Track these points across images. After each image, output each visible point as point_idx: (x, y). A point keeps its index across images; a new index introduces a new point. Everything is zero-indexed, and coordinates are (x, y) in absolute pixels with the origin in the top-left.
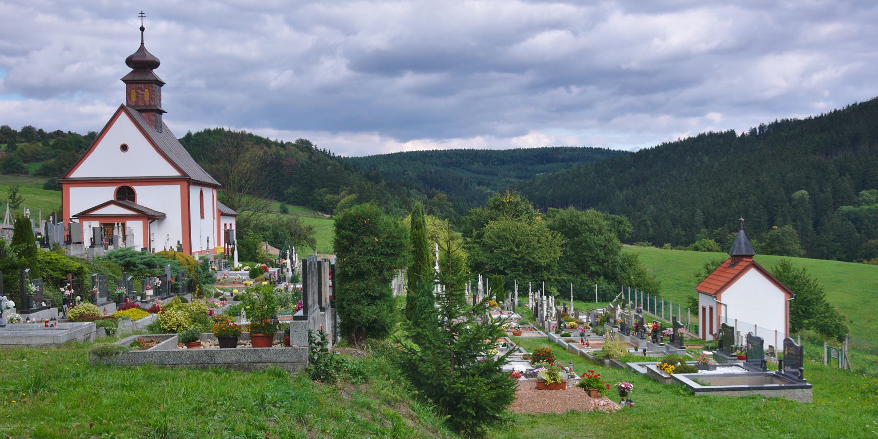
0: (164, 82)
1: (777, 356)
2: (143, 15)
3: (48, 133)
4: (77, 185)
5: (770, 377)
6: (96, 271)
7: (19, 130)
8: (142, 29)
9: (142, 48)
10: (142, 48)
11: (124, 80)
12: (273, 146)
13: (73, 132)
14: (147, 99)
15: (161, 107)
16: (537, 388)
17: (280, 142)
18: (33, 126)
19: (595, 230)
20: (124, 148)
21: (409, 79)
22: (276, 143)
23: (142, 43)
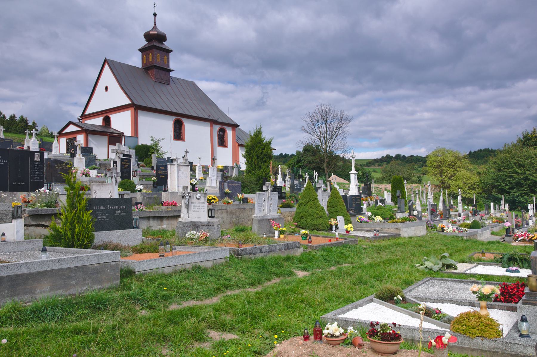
0: (172, 49)
2: (155, 5)
3: (407, 156)
4: (88, 119)
6: (405, 220)
7: (394, 156)
8: (155, 15)
9: (155, 27)
10: (155, 27)
11: (140, 50)
13: (418, 155)
14: (150, 60)
15: (169, 67)
16: (516, 311)
18: (400, 154)
20: (106, 88)
23: (155, 24)
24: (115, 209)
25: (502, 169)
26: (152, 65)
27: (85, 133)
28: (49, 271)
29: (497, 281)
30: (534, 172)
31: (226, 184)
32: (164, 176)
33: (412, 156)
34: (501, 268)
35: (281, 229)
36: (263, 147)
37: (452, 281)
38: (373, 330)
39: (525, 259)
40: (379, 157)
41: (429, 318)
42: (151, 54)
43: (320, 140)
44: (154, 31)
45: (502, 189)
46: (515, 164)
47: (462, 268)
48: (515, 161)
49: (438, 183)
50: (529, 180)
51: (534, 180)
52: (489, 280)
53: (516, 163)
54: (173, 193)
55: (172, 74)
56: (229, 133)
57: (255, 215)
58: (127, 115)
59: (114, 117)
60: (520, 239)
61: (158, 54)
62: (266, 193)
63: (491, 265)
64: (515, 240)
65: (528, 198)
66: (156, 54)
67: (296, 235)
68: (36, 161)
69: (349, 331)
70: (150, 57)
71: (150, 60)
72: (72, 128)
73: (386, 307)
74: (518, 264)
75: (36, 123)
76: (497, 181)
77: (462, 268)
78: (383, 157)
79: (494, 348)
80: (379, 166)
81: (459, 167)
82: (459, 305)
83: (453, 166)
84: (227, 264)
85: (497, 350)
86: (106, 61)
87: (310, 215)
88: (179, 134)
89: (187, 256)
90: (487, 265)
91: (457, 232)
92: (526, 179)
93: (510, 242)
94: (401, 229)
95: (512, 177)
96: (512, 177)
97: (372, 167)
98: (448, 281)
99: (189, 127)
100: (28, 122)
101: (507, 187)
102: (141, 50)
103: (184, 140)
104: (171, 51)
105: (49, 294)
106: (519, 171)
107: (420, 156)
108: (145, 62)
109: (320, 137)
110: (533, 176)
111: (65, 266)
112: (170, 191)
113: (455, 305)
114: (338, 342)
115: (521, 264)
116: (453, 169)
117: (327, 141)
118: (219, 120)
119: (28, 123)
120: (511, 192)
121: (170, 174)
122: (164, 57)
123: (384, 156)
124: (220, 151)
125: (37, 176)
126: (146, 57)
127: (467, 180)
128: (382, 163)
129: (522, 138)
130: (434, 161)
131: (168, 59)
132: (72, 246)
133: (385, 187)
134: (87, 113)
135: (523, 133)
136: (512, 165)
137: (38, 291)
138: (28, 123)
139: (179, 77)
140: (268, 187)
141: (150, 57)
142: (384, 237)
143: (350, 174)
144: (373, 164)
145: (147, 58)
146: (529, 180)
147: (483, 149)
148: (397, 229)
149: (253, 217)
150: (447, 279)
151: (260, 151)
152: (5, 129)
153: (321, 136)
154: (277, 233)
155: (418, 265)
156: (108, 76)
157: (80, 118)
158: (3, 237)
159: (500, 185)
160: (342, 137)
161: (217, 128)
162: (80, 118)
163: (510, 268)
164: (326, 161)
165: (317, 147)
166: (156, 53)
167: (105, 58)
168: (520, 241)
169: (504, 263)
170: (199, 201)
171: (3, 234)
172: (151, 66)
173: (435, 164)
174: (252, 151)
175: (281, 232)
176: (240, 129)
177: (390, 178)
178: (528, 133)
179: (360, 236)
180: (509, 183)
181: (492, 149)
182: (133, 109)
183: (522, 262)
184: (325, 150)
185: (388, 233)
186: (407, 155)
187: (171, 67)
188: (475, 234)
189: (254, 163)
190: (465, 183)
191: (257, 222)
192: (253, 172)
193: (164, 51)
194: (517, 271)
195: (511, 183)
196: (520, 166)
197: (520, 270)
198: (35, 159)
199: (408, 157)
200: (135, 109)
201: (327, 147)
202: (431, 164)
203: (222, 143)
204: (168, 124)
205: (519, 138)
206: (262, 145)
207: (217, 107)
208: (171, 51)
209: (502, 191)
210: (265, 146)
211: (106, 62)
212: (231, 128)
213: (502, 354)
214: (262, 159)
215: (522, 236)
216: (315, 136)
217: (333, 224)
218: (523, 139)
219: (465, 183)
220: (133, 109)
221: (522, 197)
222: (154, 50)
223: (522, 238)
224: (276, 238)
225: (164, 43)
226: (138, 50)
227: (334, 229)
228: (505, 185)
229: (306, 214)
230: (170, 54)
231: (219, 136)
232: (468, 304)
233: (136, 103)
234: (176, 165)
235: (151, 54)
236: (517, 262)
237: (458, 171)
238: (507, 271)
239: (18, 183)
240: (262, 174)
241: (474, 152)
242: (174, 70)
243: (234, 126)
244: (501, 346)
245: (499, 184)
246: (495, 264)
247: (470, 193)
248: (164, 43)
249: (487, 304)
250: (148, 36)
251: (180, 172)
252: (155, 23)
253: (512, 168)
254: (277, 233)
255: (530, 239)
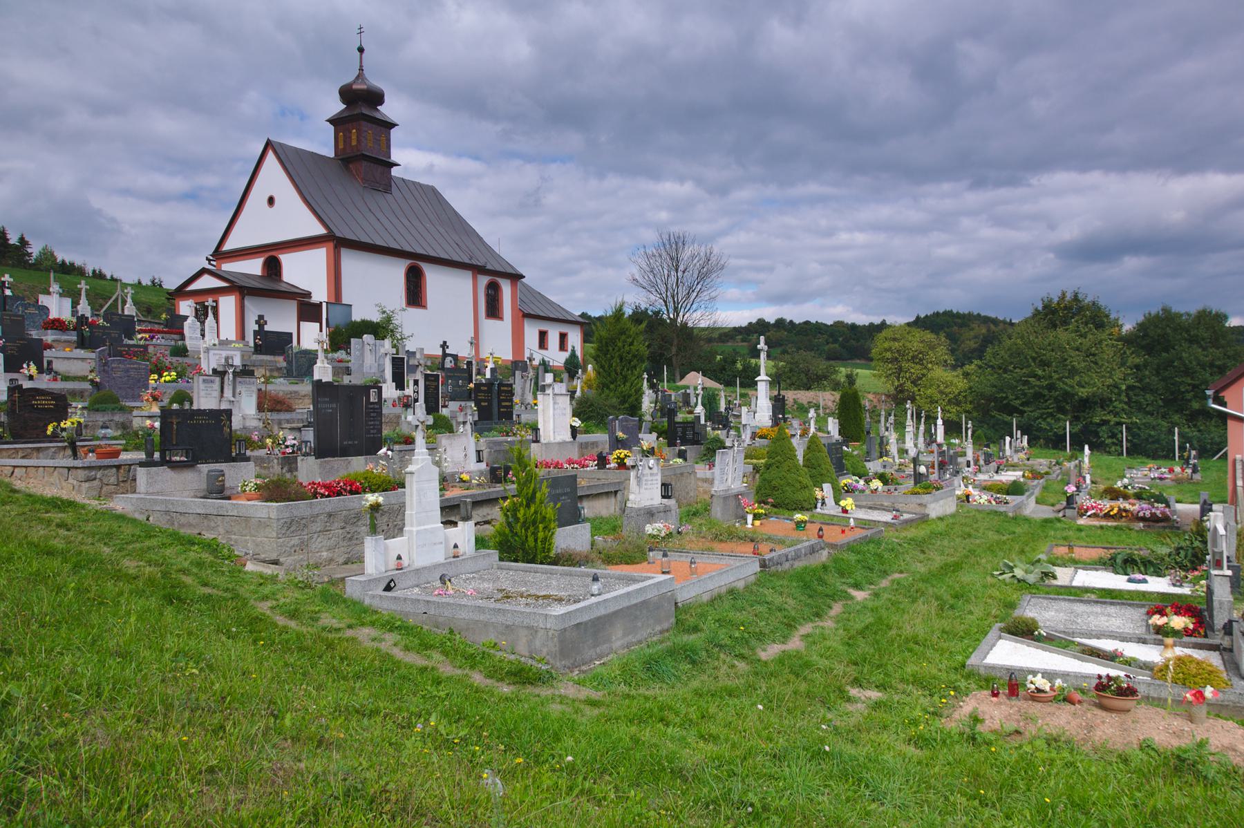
1: (1021, 408)
2: (362, 30)
5: (24, 470)
7: (772, 322)
8: (361, 50)
9: (361, 76)
10: (361, 76)
11: (331, 121)
12: (1001, 324)
13: (819, 321)
14: (354, 143)
15: (390, 157)
17: (1008, 321)
18: (784, 317)
19: (1203, 339)
20: (271, 201)
21: (1131, 263)
22: (1004, 322)
23: (361, 69)
24: (559, 494)
25: (1011, 368)
26: (359, 153)
27: (238, 294)
28: (621, 609)
29: (1129, 599)
30: (1067, 375)
31: (617, 422)
32: (486, 404)
33: (807, 323)
34: (1113, 574)
35: (756, 511)
36: (630, 340)
37: (1065, 600)
38: (1101, 683)
39: (1150, 562)
40: (744, 324)
41: (1113, 663)
42: (354, 131)
43: (665, 302)
44: (361, 84)
45: (1008, 405)
46: (1034, 359)
47: (1063, 576)
48: (1034, 355)
49: (892, 391)
50: (1056, 389)
51: (1065, 390)
52: (1116, 597)
53: (1036, 358)
54: (548, 445)
55: (395, 172)
56: (506, 288)
57: (715, 489)
58: (318, 257)
59: (287, 259)
60: (1089, 513)
61: (370, 131)
62: (730, 452)
63: (1097, 570)
64: (1082, 515)
65: (1053, 421)
66: (366, 131)
67: (772, 519)
68: (373, 403)
69: (1057, 684)
70: (354, 137)
71: (354, 143)
72: (207, 282)
73: (1028, 646)
74: (1139, 569)
75: (26, 239)
76: (1002, 390)
77: (1063, 576)
78: (750, 323)
79: (1222, 701)
80: (743, 341)
81: (931, 362)
82: (1123, 641)
83: (921, 360)
84: (758, 583)
85: (1227, 703)
86: (269, 145)
87: (788, 484)
88: (415, 295)
89: (721, 574)
90: (1091, 569)
91: (994, 503)
92: (1051, 387)
93: (1074, 519)
94: (928, 505)
95: (1026, 383)
96: (1026, 383)
97: (730, 344)
98: (1059, 599)
99: (435, 279)
100: (9, 236)
101: (1018, 402)
102: (334, 121)
103: (424, 307)
104: (393, 125)
105: (622, 641)
106: (1040, 373)
107: (822, 323)
108: (341, 147)
109: (664, 296)
110: (1063, 382)
111: (634, 602)
112: (542, 440)
113: (1118, 642)
114: (1050, 699)
115: (1142, 569)
116: (921, 365)
117: (678, 304)
118: (489, 267)
119: (8, 240)
120: (1025, 412)
121: (543, 410)
122: (381, 136)
123: (754, 321)
124: (489, 325)
125: (373, 429)
126: (344, 135)
127: (946, 387)
128: (749, 335)
129: (1040, 308)
130: (886, 350)
131: (389, 140)
132: (532, 561)
133: (794, 397)
134: (228, 246)
135: (1042, 300)
136: (1028, 361)
137: (614, 638)
138: (8, 240)
139: (422, 182)
140: (733, 441)
141: (354, 137)
142: (912, 521)
143: (757, 382)
144: (731, 338)
145: (347, 139)
146: (1056, 389)
147: (941, 312)
148: (920, 505)
149: (713, 493)
150: (1056, 597)
151: (627, 348)
152: (88, 287)
153: (667, 295)
154: (750, 518)
155: (998, 573)
156: (273, 176)
157: (211, 258)
158: (456, 549)
159: (1006, 398)
160: (707, 298)
161: (484, 280)
162: (211, 258)
163: (1132, 576)
164: (675, 342)
165: (657, 313)
166: (366, 129)
167: (268, 139)
168: (1089, 516)
169: (1117, 567)
170: (651, 471)
171: (456, 546)
172: (357, 156)
173: (888, 355)
174: (611, 349)
175: (756, 517)
176: (524, 285)
177: (791, 375)
178: (1051, 301)
179: (879, 522)
180: (1022, 395)
181: (957, 313)
182: (331, 245)
183: (1145, 566)
184: (674, 321)
185: (915, 514)
186: (797, 321)
187: (395, 157)
188: (1019, 507)
189: (615, 370)
190: (941, 392)
191: (722, 501)
192: (612, 386)
193: (374, 123)
194: (1145, 581)
195: (1025, 394)
196: (1044, 364)
197: (1147, 578)
198: (372, 400)
199: (800, 324)
200: (336, 247)
201: (678, 315)
202: (880, 354)
203: (494, 310)
204: (394, 274)
205: (1036, 310)
206: (629, 336)
207: (481, 239)
208: (393, 125)
209: (1011, 410)
210: (634, 338)
211: (269, 147)
212: (508, 282)
213: (1234, 707)
214: (630, 363)
215: (1093, 508)
216: (655, 293)
217: (819, 497)
218: (1043, 310)
219: (941, 392)
220: (331, 245)
221: (1045, 419)
222: (363, 123)
223: (1093, 511)
224: (749, 526)
225: (379, 108)
226: (327, 121)
227: (819, 505)
228: (1014, 397)
229: (782, 482)
230: (392, 131)
231: (488, 295)
232: (1137, 640)
233: (338, 234)
234: (551, 395)
235: (354, 131)
236: (1137, 566)
237: (929, 370)
238: (1130, 581)
239: (350, 443)
240: (631, 390)
241: (924, 318)
242: (399, 163)
243: (515, 277)
244: (1232, 698)
245: (1004, 395)
246: (1102, 569)
247: (951, 410)
248: (379, 108)
249: (1174, 642)
250: (347, 94)
251: (556, 406)
252: (361, 66)
253: (1029, 366)
254: (750, 518)
255: (1105, 514)
